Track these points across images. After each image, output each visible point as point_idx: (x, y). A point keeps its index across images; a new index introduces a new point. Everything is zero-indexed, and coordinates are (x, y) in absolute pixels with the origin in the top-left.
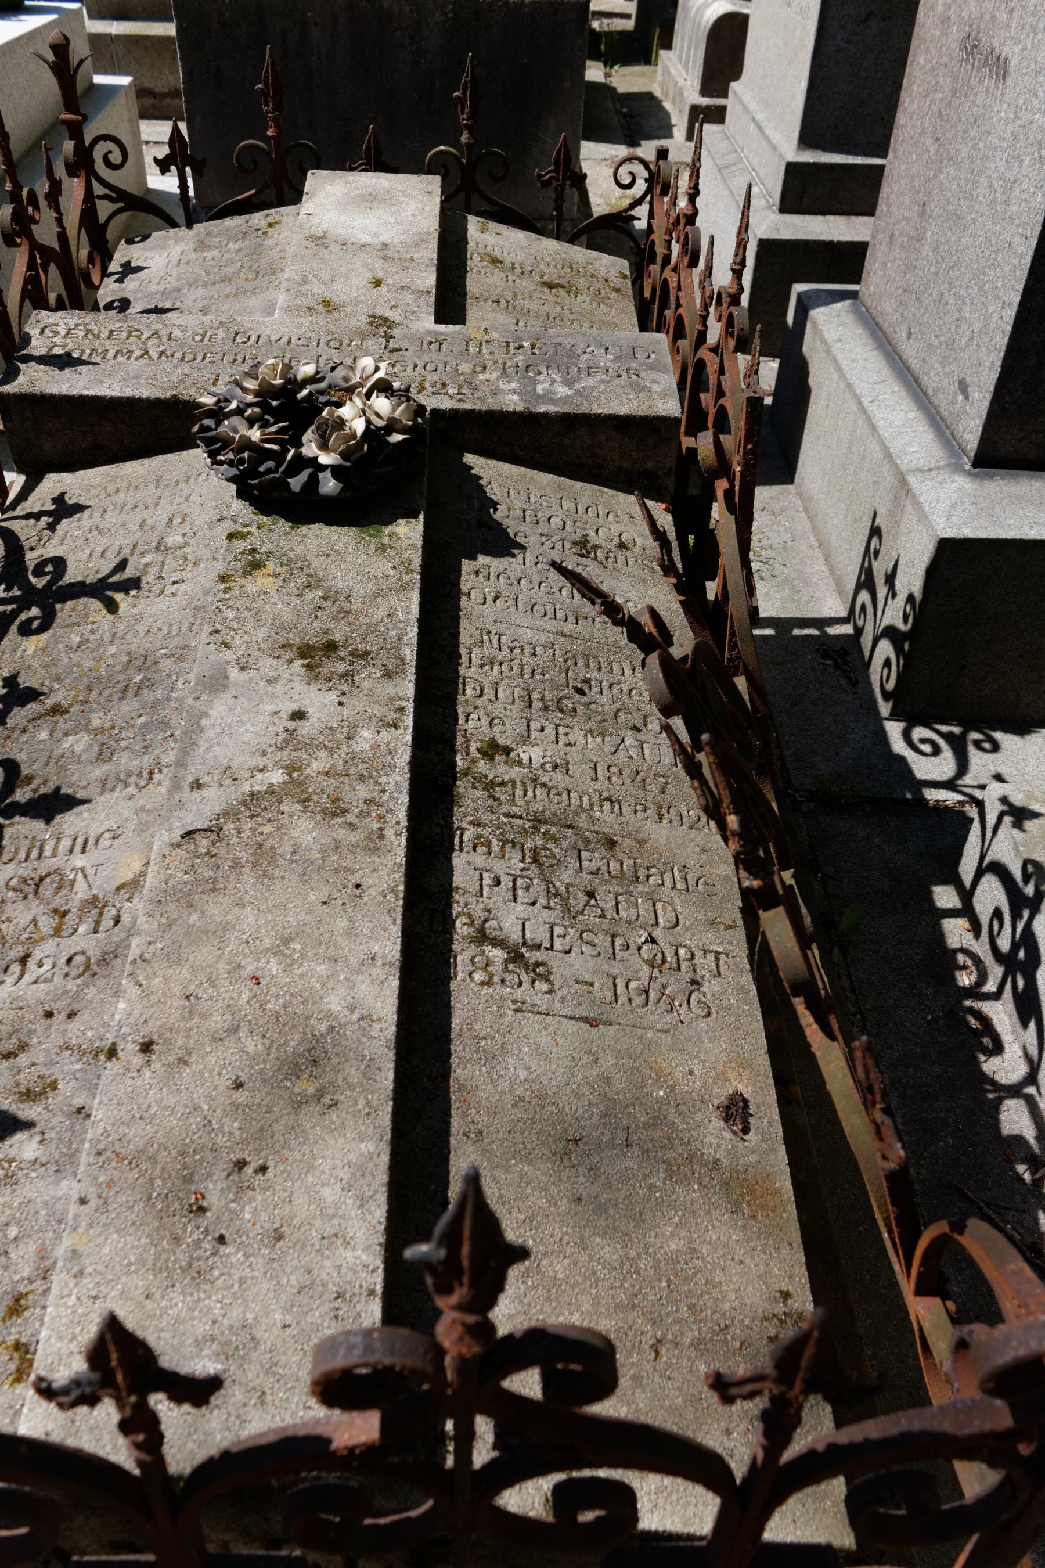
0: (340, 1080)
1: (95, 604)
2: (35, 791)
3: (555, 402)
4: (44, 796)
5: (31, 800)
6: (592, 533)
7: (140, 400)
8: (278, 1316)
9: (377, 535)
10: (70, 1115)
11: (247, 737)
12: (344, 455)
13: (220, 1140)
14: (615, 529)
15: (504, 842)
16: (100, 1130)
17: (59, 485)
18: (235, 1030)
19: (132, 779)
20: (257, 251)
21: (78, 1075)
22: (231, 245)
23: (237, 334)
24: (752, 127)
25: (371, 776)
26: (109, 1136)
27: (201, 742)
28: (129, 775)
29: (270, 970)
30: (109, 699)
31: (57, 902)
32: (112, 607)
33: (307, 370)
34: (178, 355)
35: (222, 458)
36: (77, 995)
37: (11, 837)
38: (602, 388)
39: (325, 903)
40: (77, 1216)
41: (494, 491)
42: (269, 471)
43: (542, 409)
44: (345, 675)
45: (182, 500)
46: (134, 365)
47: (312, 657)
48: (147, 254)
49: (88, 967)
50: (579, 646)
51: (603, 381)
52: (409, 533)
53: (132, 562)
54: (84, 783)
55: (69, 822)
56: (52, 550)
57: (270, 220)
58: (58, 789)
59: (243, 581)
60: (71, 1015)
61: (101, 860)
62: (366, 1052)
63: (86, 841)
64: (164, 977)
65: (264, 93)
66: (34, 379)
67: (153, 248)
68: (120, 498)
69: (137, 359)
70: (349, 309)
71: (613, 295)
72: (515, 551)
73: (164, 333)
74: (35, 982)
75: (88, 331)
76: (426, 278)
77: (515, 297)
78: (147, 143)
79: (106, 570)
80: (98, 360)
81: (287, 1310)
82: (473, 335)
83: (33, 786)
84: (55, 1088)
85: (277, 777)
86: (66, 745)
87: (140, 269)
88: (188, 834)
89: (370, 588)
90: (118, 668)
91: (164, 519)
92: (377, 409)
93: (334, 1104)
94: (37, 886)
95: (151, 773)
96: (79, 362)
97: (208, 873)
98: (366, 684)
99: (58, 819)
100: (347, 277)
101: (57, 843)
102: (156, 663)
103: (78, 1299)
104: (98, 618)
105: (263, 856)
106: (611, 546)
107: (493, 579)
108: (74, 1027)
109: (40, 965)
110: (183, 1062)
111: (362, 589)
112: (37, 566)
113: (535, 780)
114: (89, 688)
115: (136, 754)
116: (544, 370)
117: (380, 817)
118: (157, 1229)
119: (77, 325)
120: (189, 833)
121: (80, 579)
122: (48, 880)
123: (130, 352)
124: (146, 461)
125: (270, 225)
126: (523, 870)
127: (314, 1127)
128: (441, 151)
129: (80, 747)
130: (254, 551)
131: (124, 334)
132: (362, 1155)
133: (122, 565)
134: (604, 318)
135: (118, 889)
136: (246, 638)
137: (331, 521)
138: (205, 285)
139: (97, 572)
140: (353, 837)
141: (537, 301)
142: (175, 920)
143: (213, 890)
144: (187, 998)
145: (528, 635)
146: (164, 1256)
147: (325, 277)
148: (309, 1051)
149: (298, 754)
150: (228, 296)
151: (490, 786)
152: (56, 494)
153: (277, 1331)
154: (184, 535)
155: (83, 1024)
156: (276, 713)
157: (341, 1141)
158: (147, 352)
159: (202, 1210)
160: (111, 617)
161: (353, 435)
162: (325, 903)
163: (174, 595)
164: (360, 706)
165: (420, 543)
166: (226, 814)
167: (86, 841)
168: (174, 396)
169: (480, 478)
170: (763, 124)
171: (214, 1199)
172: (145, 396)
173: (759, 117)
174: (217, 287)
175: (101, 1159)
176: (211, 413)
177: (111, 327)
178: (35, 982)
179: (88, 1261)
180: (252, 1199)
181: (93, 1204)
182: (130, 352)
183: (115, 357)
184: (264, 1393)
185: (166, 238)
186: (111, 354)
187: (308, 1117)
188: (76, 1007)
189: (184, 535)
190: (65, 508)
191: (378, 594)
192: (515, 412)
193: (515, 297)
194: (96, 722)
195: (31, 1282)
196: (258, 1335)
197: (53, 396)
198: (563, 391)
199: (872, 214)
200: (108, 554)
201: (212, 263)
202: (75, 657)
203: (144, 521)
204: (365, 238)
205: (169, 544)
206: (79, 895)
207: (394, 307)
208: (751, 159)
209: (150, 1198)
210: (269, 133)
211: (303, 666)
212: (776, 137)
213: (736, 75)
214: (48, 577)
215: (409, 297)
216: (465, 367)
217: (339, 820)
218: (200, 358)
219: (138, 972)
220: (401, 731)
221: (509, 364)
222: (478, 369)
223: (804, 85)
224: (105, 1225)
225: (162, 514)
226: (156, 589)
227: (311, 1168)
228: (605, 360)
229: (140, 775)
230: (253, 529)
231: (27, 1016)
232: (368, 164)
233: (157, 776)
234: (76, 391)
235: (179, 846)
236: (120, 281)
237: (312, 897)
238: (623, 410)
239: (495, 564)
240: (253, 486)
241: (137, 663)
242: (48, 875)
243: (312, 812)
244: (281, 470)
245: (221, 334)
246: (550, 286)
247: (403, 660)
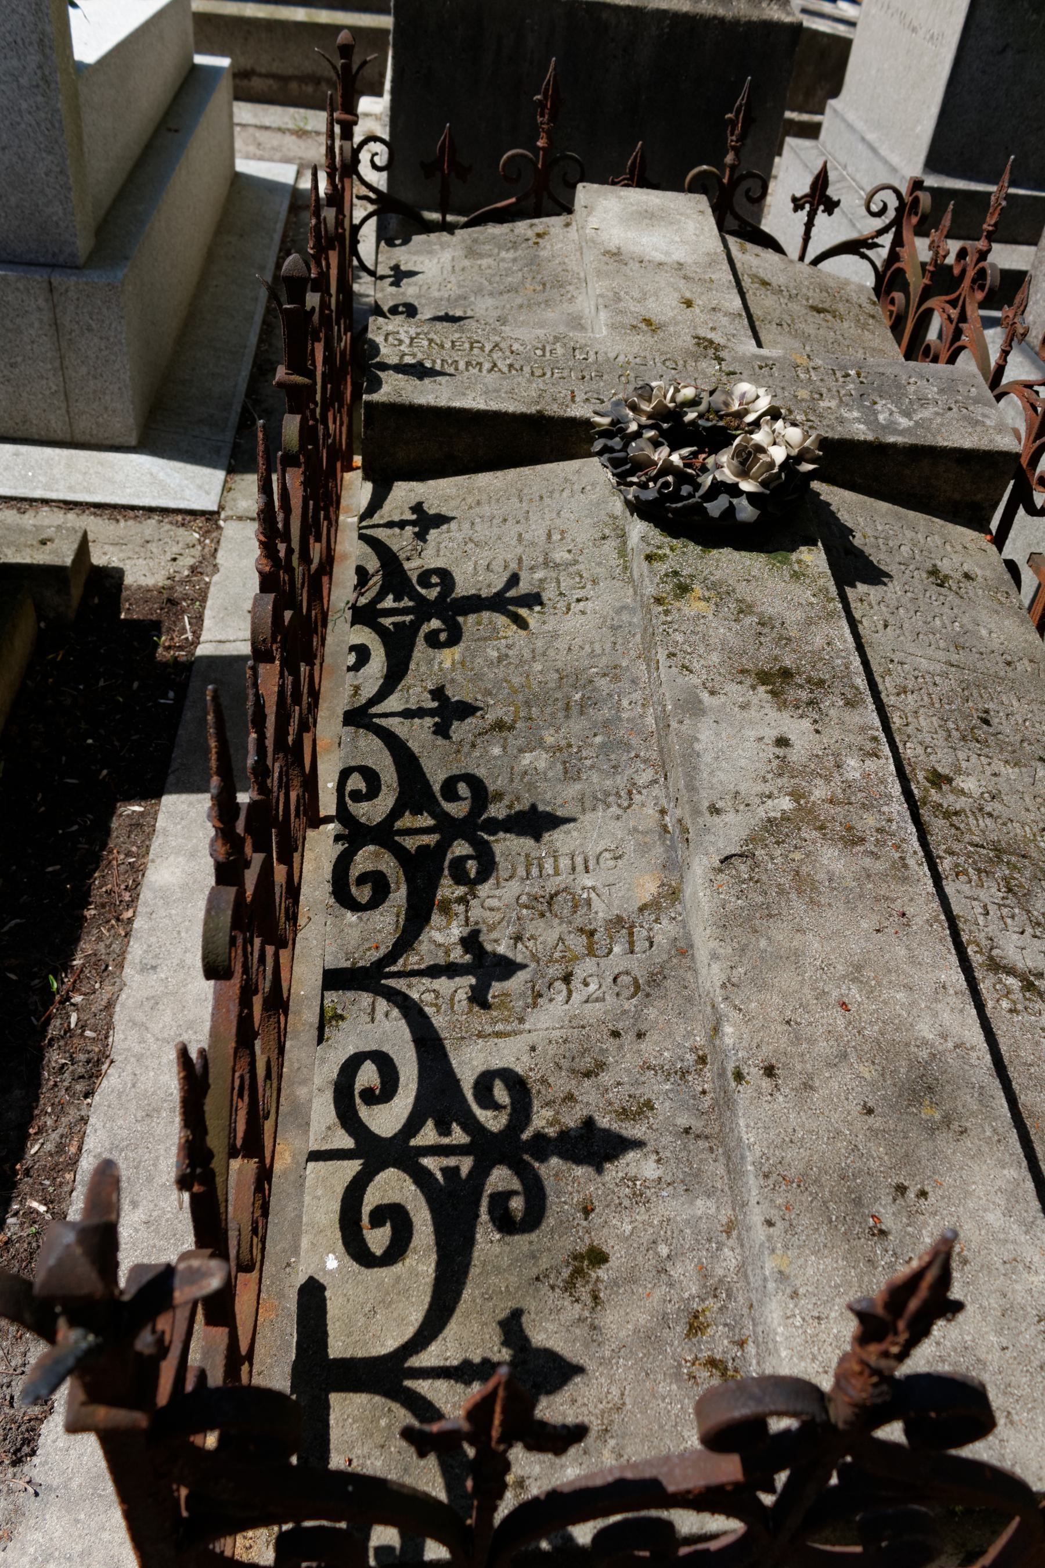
0: (960, 1108)
1: (501, 620)
2: (510, 807)
3: (901, 433)
4: (520, 813)
5: (509, 816)
6: (939, 563)
7: (506, 414)
8: (993, 1338)
9: (785, 561)
10: (678, 1135)
11: (743, 762)
12: (763, 484)
13: (874, 1165)
14: (957, 559)
15: (979, 871)
16: (758, 1154)
17: (412, 494)
18: (844, 1056)
19: (611, 799)
20: (534, 263)
21: (671, 1095)
22: (503, 254)
23: (574, 349)
24: (861, 147)
25: (872, 806)
26: (768, 1159)
27: (702, 767)
28: (607, 794)
29: (854, 997)
30: (553, 715)
31: (579, 920)
32: (521, 623)
33: (688, 393)
34: (527, 369)
35: (635, 479)
36: (638, 1016)
37: (502, 854)
38: (939, 420)
39: (878, 931)
40: (769, 1238)
41: (844, 517)
42: (691, 495)
43: (891, 439)
44: (810, 703)
45: (554, 515)
46: (491, 379)
47: (774, 684)
48: (415, 258)
49: (637, 987)
50: (968, 676)
51: (937, 414)
52: (813, 558)
53: (524, 575)
54: (559, 801)
55: (557, 837)
56: (432, 562)
57: (540, 229)
58: (534, 807)
59: (677, 604)
60: (640, 1035)
61: (611, 880)
62: (974, 1080)
63: (586, 861)
64: (758, 1001)
65: (541, 104)
66: (394, 388)
67: (418, 253)
68: (486, 510)
69: (490, 371)
70: (671, 329)
71: (871, 321)
72: (885, 580)
73: (503, 345)
74: (586, 1001)
75: (431, 341)
76: (732, 301)
77: (793, 320)
78: (243, 126)
79: (499, 584)
80: (452, 370)
81: (999, 1333)
82: (799, 361)
83: (506, 801)
84: (652, 1108)
85: (786, 804)
86: (526, 762)
87: (412, 274)
88: (726, 859)
89: (799, 615)
90: (552, 685)
91: (542, 533)
92: (787, 438)
93: (964, 1131)
94: (550, 904)
95: (630, 793)
96: (432, 373)
97: (760, 899)
98: (832, 712)
99: (546, 837)
100: (656, 295)
101: (556, 861)
102: (591, 681)
103: (804, 1319)
104: (510, 634)
105: (803, 883)
106: (958, 575)
107: (876, 607)
108: (648, 1047)
109: (586, 984)
110: (808, 1086)
111: (794, 617)
112: (420, 576)
113: (981, 810)
114: (528, 704)
115: (606, 774)
116: (878, 399)
117: (897, 847)
118: (849, 1251)
119: (418, 334)
120: (727, 858)
121: (473, 592)
122: (559, 898)
123: (480, 364)
124: (499, 474)
125: (539, 235)
126: (1003, 898)
127: (954, 1153)
128: (705, 171)
129: (542, 765)
130: (676, 573)
131: (467, 346)
132: (1008, 1182)
133: (514, 580)
134: (872, 344)
135: (641, 909)
136: (702, 662)
137: (739, 546)
138: (491, 294)
139: (489, 586)
140: (880, 866)
141: (812, 324)
142: (747, 945)
143: (770, 916)
144: (788, 1022)
145: (924, 664)
146: (866, 1279)
147: (636, 294)
148: (921, 1078)
149: (797, 780)
150: (521, 306)
151: (947, 815)
152: (413, 504)
153: (998, 1354)
154: (569, 551)
155: (656, 1043)
156: (762, 739)
157: (985, 1167)
158: (495, 365)
159: (883, 1233)
160: (523, 633)
161: (772, 464)
162: (878, 931)
163: (583, 613)
164: (837, 734)
165: (829, 572)
166: (751, 839)
167: (586, 861)
168: (539, 412)
169: (829, 505)
170: (876, 145)
171: (888, 1222)
172: (511, 409)
173: (870, 137)
174: (506, 296)
175: (771, 1182)
176: (607, 434)
177: (451, 338)
178: (586, 1001)
179: (798, 1282)
180: (925, 1224)
181: (780, 1224)
182: (480, 364)
183: (467, 369)
184: (1009, 1413)
185: (429, 243)
186: (462, 365)
187: (944, 1140)
188: (643, 1027)
189: (569, 551)
190: (425, 521)
191: (809, 622)
192: (865, 442)
193: (793, 320)
194: (550, 740)
195: (703, 1300)
196: (983, 1357)
197: (421, 407)
198: (904, 422)
199: (1034, 243)
200: (494, 566)
201: (489, 271)
202: (500, 672)
203: (520, 535)
204: (659, 257)
205: (558, 561)
206: (601, 915)
207: (713, 329)
208: (858, 177)
209: (831, 1221)
210: (540, 144)
211: (767, 692)
212: (895, 159)
213: (835, 91)
214: (438, 589)
215: (725, 320)
216: (803, 394)
217: (861, 849)
218: (549, 374)
219: (732, 996)
220: (883, 761)
221: (843, 392)
222: (817, 396)
223: (935, 110)
224: (799, 1247)
225: (536, 531)
226: (561, 605)
227: (967, 1194)
228: (932, 392)
229: (618, 795)
230: (668, 551)
231: (593, 1034)
232: (631, 179)
233: (637, 797)
234: (443, 402)
235: (721, 871)
236: (396, 284)
237: (864, 925)
238: (967, 444)
239: (873, 592)
240: (669, 510)
241: (571, 681)
242: (557, 894)
243: (832, 839)
244: (697, 495)
245: (560, 351)
246: (819, 311)
247: (857, 689)
